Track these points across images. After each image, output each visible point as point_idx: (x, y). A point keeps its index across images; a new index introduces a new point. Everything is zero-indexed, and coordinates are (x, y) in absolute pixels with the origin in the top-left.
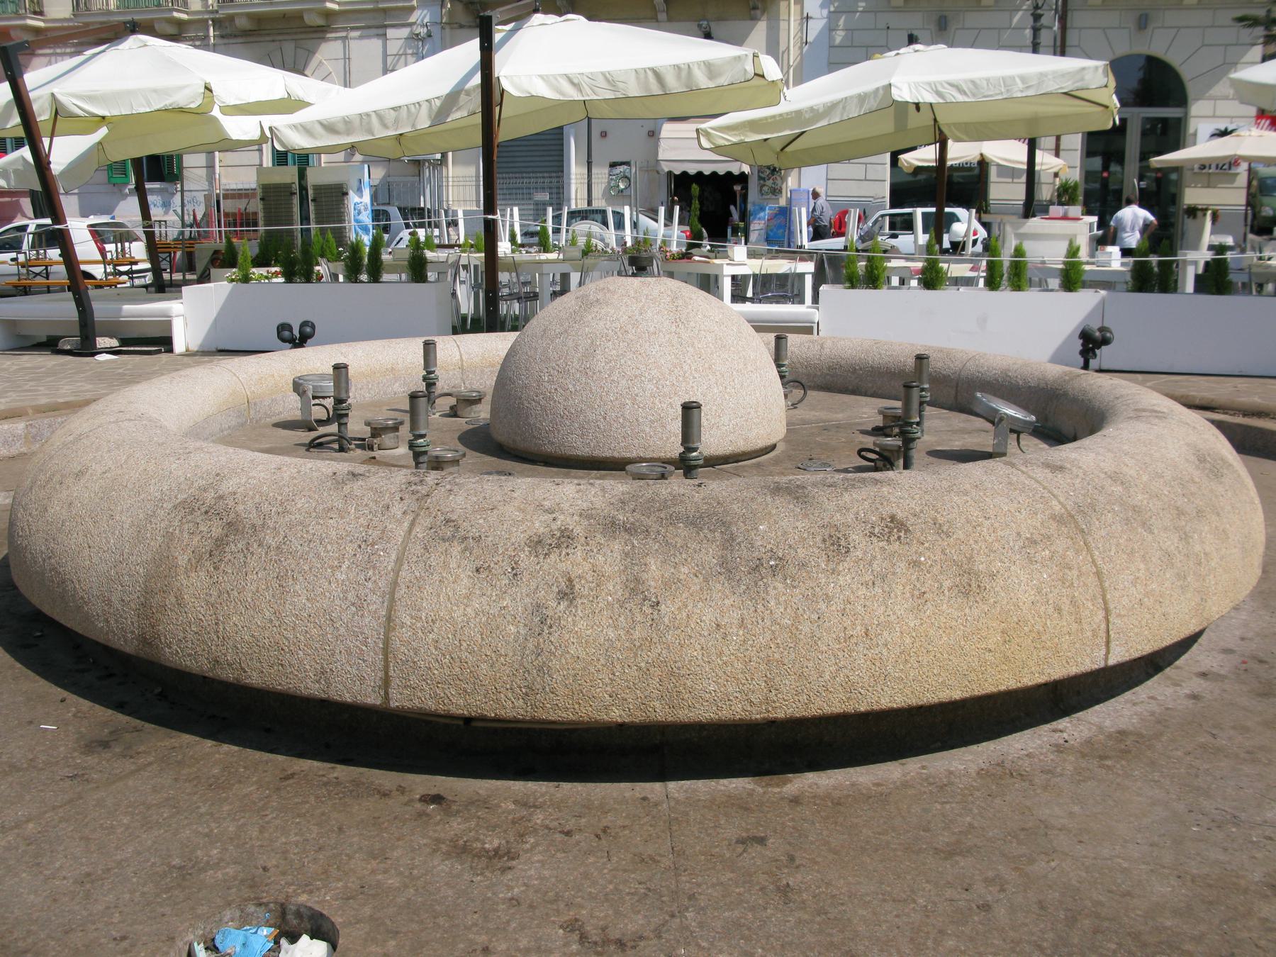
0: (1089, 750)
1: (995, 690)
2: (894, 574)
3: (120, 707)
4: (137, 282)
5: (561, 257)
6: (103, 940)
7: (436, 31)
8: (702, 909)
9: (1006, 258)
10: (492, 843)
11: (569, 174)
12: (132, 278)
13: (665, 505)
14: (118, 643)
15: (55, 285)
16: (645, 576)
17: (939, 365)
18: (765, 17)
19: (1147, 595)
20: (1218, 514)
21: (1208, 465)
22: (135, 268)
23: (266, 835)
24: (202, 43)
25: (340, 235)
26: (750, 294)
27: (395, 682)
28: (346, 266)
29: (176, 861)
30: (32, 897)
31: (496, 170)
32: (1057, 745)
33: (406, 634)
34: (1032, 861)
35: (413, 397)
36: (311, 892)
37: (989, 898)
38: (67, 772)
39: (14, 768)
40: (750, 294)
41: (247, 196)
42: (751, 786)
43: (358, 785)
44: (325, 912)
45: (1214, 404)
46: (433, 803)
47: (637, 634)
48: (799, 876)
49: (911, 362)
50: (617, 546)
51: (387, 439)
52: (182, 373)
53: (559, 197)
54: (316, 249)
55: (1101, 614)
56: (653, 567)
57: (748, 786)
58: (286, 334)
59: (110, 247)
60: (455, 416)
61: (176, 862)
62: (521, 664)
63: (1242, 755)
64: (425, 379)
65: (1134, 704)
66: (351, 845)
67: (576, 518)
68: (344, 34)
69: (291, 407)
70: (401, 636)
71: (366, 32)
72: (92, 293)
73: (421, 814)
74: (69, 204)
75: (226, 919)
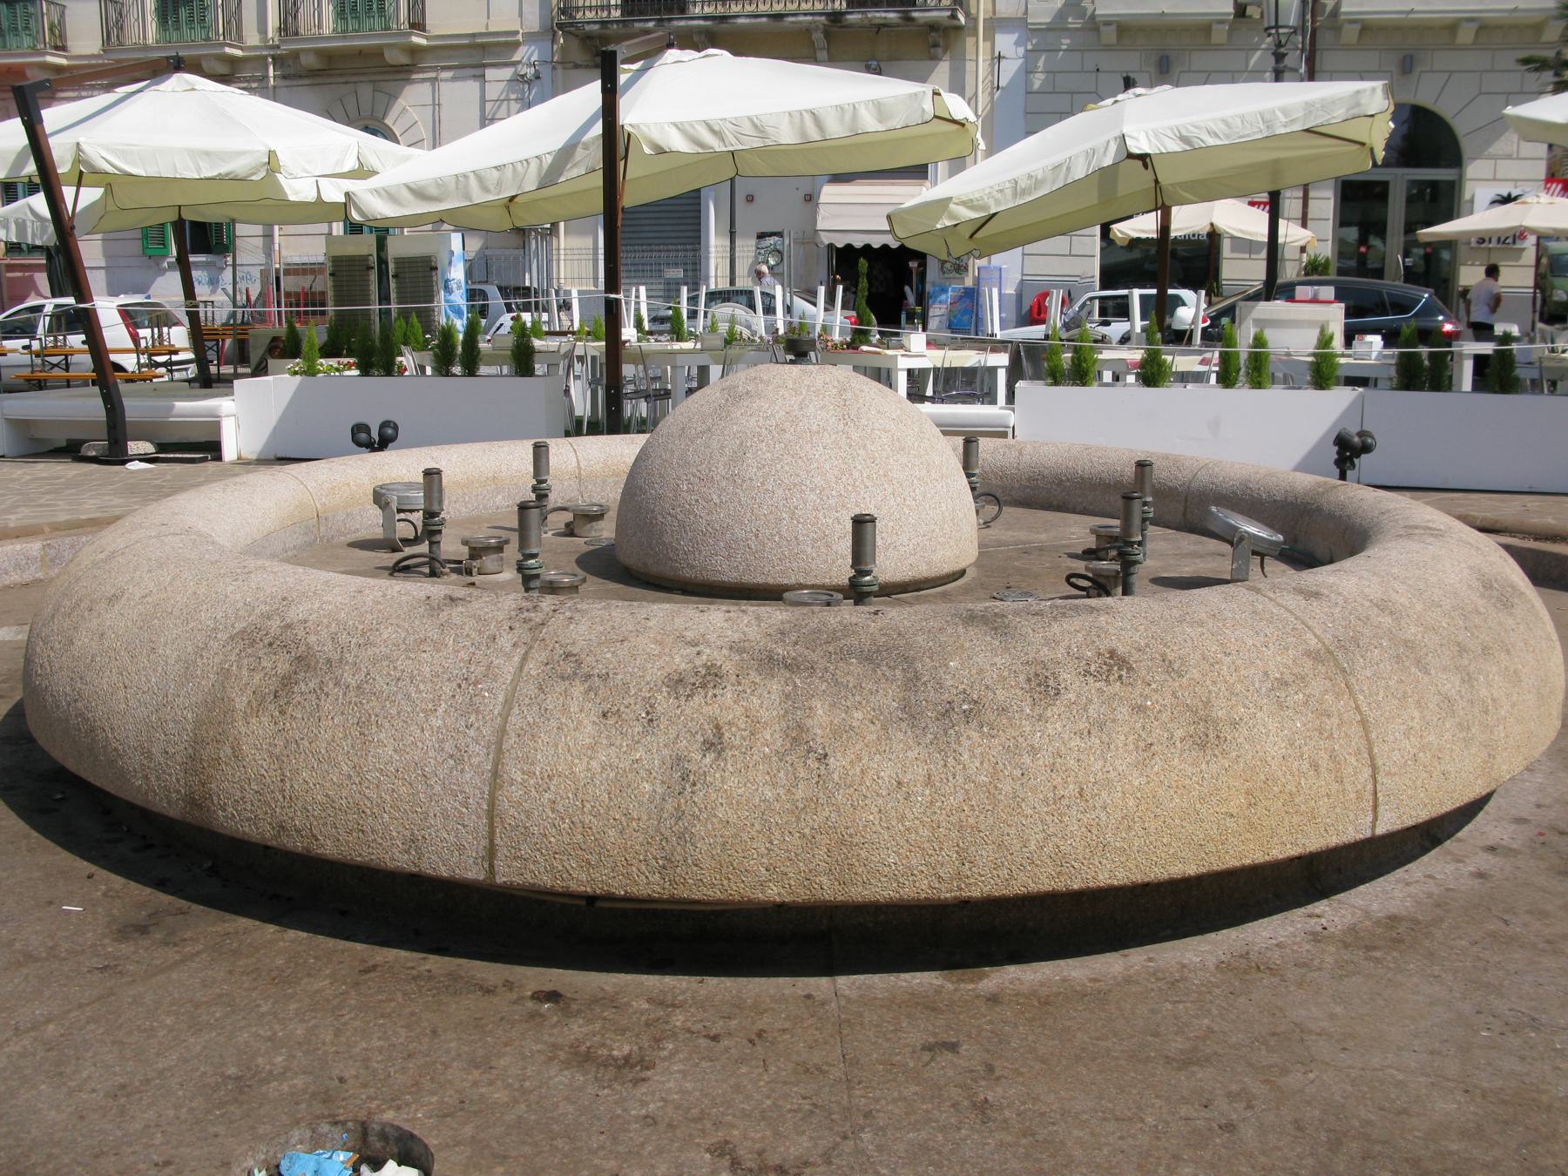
0: (1353, 939)
1: (1237, 864)
2: (1114, 721)
3: (161, 884)
4: (177, 375)
5: (699, 346)
6: (141, 1166)
7: (546, 72)
8: (881, 1129)
9: (1243, 348)
10: (622, 1049)
11: (708, 247)
12: (171, 371)
13: (833, 637)
14: (160, 805)
15: (77, 378)
16: (809, 722)
17: (1164, 475)
18: (947, 57)
19: (1422, 749)
20: (1508, 651)
21: (1495, 593)
22: (174, 358)
23: (343, 1039)
24: (259, 87)
25: (426, 317)
26: (929, 392)
27: (502, 852)
28: (436, 355)
29: (232, 1071)
30: (53, 1113)
31: (620, 242)
32: (1314, 934)
33: (516, 793)
34: (1285, 1072)
35: (523, 508)
36: (399, 1108)
37: (1234, 1117)
38: (96, 962)
39: (30, 957)
40: (929, 392)
41: (313, 271)
42: (938, 982)
43: (455, 980)
44: (416, 1132)
45: (1498, 526)
46: (548, 1000)
47: (799, 794)
48: (999, 1090)
49: (1130, 471)
50: (775, 686)
51: (489, 561)
52: (237, 479)
53: (695, 276)
54: (398, 335)
55: (1367, 772)
56: (820, 712)
57: (935, 982)
58: (363, 436)
59: (144, 333)
60: (572, 534)
61: (232, 1071)
62: (658, 830)
63: (1541, 946)
64: (534, 489)
65: (1407, 884)
66: (448, 1051)
67: (725, 651)
68: (433, 75)
69: (371, 522)
70: (510, 795)
71: (460, 72)
72: (123, 387)
73: (533, 1015)
74: (96, 281)
75: (293, 1141)
